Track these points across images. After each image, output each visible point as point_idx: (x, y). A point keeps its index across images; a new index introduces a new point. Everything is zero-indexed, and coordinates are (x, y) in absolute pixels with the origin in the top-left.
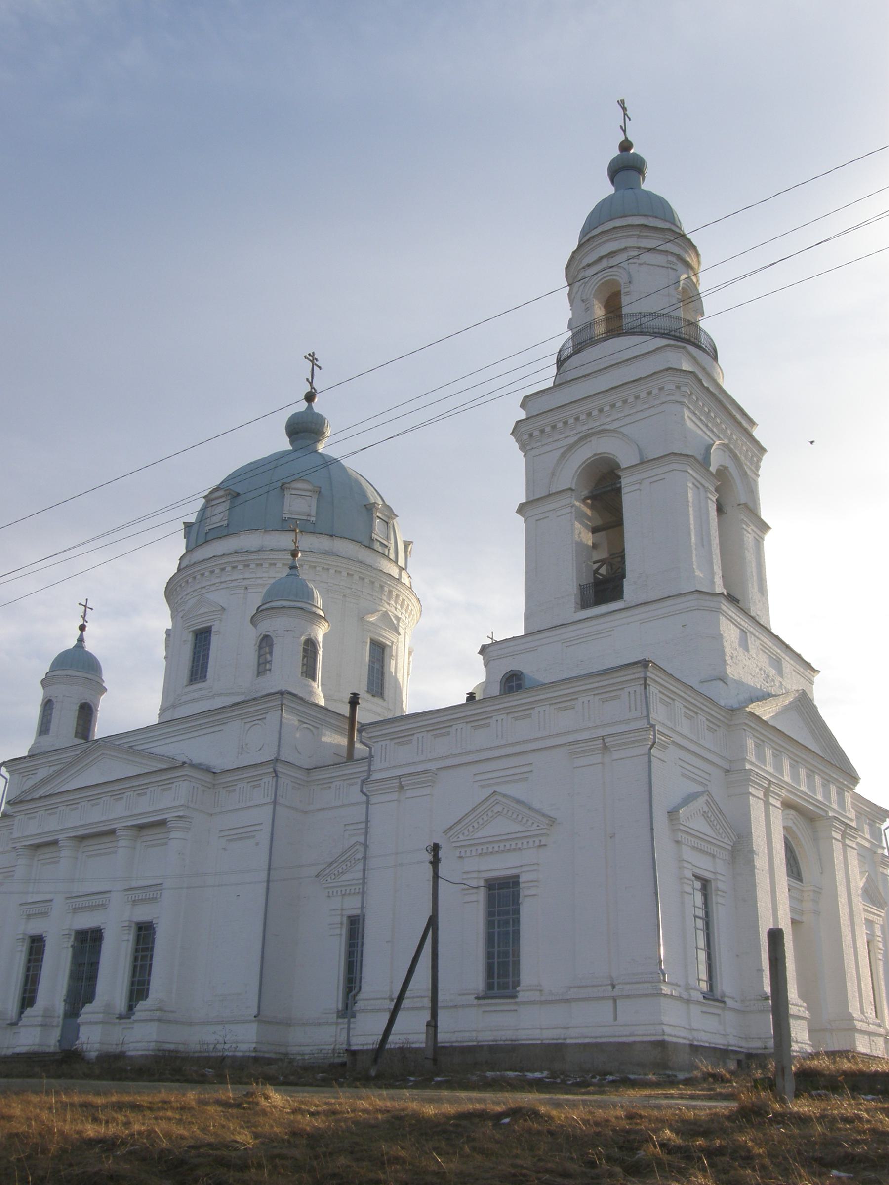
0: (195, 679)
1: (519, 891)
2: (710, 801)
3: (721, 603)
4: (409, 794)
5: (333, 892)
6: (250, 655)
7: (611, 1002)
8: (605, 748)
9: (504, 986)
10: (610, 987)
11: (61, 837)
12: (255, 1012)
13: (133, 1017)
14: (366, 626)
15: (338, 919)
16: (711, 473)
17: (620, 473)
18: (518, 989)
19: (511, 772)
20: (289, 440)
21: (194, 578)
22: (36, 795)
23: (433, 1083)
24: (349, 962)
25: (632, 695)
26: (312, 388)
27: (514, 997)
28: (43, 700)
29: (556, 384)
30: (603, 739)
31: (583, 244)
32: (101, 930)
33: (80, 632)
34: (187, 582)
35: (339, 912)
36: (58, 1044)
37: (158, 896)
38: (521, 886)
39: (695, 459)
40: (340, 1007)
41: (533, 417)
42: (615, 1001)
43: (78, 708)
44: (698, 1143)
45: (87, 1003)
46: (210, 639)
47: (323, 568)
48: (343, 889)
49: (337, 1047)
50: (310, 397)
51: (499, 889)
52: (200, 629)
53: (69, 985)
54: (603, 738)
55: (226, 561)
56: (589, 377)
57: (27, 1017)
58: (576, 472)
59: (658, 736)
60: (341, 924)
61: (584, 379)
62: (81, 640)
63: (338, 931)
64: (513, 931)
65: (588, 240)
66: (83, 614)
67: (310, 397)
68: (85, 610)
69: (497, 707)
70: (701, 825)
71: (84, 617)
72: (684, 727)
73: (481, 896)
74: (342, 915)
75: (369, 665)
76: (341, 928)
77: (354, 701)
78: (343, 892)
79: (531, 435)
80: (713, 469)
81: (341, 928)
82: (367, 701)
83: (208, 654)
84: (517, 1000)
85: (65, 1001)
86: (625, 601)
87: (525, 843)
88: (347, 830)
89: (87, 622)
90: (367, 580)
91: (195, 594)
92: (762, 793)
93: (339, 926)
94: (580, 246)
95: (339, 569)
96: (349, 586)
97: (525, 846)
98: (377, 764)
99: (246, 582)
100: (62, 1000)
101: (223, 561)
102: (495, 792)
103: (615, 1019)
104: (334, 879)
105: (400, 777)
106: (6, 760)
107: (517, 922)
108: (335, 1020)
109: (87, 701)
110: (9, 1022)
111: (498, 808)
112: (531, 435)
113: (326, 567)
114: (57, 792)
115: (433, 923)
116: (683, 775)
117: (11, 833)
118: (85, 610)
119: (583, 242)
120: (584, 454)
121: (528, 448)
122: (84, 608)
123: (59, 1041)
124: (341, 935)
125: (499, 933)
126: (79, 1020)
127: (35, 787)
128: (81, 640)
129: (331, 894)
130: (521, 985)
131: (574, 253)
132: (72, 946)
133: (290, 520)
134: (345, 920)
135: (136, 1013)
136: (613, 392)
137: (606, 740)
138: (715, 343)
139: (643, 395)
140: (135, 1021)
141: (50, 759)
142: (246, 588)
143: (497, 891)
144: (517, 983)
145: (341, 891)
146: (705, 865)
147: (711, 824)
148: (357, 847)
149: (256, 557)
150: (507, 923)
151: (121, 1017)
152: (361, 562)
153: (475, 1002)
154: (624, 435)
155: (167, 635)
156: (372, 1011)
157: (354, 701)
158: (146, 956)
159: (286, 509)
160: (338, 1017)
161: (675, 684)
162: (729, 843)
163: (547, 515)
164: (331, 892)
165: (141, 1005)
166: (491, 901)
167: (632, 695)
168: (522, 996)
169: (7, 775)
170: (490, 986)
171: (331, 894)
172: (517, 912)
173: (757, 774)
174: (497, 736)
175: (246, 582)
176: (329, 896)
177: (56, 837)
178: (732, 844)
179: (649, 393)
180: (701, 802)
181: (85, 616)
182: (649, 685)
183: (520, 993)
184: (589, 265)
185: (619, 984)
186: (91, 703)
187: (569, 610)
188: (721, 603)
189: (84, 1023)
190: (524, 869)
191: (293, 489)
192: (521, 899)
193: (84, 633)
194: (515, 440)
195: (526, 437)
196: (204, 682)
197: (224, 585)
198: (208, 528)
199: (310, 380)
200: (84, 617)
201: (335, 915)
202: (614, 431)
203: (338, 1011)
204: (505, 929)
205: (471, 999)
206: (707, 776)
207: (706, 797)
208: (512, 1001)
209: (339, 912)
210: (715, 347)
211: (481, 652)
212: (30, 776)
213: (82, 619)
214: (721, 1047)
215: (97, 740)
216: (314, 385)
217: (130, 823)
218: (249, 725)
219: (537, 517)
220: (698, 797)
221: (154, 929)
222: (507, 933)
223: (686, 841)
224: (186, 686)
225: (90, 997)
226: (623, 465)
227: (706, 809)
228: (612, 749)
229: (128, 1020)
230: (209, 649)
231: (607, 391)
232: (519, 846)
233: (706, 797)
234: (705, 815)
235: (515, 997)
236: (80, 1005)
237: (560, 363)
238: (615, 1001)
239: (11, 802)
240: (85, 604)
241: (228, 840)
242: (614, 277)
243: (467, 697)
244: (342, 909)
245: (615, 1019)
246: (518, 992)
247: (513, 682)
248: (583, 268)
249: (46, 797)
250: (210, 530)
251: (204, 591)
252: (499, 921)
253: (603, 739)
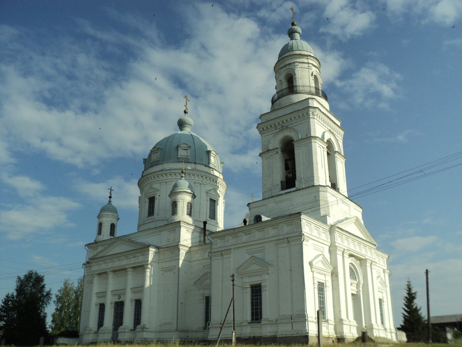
0: (150, 215)
1: (261, 289)
2: (323, 257)
3: (327, 189)
4: (225, 256)
5: (200, 288)
6: (169, 207)
7: (291, 324)
8: (288, 241)
9: (257, 319)
10: (290, 319)
11: (108, 271)
12: (176, 328)
13: (136, 330)
14: (208, 195)
15: (202, 298)
16: (325, 142)
17: (294, 143)
18: (262, 320)
19: (257, 249)
20: (179, 127)
21: (148, 179)
22: (99, 256)
23: (22, 288)
24: (206, 311)
25: (297, 224)
26: (186, 108)
27: (260, 322)
28: (98, 223)
29: (271, 110)
30: (287, 239)
31: (279, 60)
32: (123, 302)
33: (109, 199)
34: (146, 181)
35: (202, 295)
36: (111, 339)
37: (142, 290)
38: (262, 287)
39: (319, 138)
40: (204, 326)
41: (263, 123)
42: (292, 323)
43: (110, 225)
44: (75, 326)
45: (120, 326)
46: (154, 201)
47: (193, 175)
48: (204, 287)
49: (204, 339)
51: (255, 288)
52: (151, 197)
53: (114, 320)
54: (287, 238)
55: (159, 173)
56: (282, 109)
57: (101, 330)
58: (280, 140)
59: (305, 237)
60: (203, 299)
61: (281, 109)
62: (110, 201)
63: (202, 301)
64: (260, 308)
65: (281, 59)
66: (110, 192)
68: (111, 191)
69: (253, 227)
70: (320, 265)
71: (110, 193)
72: (315, 233)
73: (249, 290)
74: (203, 296)
75: (210, 208)
76: (203, 300)
77: (205, 223)
78: (204, 288)
79: (263, 129)
80: (325, 141)
81: (203, 300)
82: (209, 221)
83: (154, 206)
84: (261, 324)
85: (113, 325)
86: (296, 188)
87: (263, 273)
88: (204, 267)
89: (111, 195)
90: (208, 178)
91: (149, 185)
92: (341, 253)
93: (203, 300)
94: (278, 61)
95: (198, 175)
96: (202, 181)
97: (263, 274)
98: (214, 247)
99: (166, 181)
100: (111, 325)
101: (158, 174)
102: (253, 256)
103: (292, 329)
104: (200, 284)
105: (221, 251)
106: (87, 244)
107: (261, 299)
108: (202, 330)
109: (113, 223)
110: (95, 332)
111: (254, 261)
112: (263, 129)
113: (193, 174)
114: (106, 255)
115: (233, 299)
116: (314, 249)
117: (91, 269)
118: (111, 191)
119: (279, 59)
120: (281, 136)
121: (262, 133)
122: (112, 189)
123: (112, 338)
124: (203, 303)
125: (255, 302)
126: (118, 331)
127: (98, 254)
128: (110, 201)
129: (199, 289)
130: (263, 319)
131: (276, 63)
132: (114, 307)
133: (181, 158)
134: (204, 297)
135: (137, 329)
136: (290, 114)
137: (288, 239)
138: (326, 94)
139: (301, 115)
140: (136, 332)
141: (102, 244)
142: (166, 183)
143: (254, 289)
144: (261, 318)
145: (203, 288)
146: (321, 278)
147: (324, 265)
148: (208, 273)
149: (169, 172)
150: (257, 299)
151: (131, 330)
152: (206, 172)
153: (248, 324)
154: (295, 129)
155: (139, 199)
156: (215, 328)
157: (205, 223)
158: (139, 310)
159: (179, 154)
160: (203, 330)
161: (311, 219)
162: (330, 270)
163: (269, 157)
164: (199, 288)
165: (138, 327)
166: (252, 292)
167: (297, 224)
168: (263, 322)
169: (88, 249)
170: (252, 319)
171: (199, 289)
172: (261, 295)
173: (340, 247)
174: (253, 237)
175: (166, 181)
176: (199, 290)
177: (106, 271)
178: (331, 271)
179: (303, 115)
180: (320, 258)
182: (302, 220)
183: (262, 321)
184: (282, 68)
185: (294, 318)
186: (114, 223)
187: (278, 190)
188: (327, 189)
189: (119, 332)
190: (263, 281)
191: (181, 147)
192: (262, 291)
193: (111, 199)
194: (257, 130)
195: (261, 129)
196: (153, 216)
197: (158, 182)
198: (152, 161)
199: (186, 105)
200: (110, 193)
201: (148, 237)
202: (291, 128)
203: (203, 328)
204: (257, 301)
205: (246, 324)
206: (323, 249)
207: (322, 256)
208: (260, 324)
209: (202, 295)
210: (326, 96)
211: (248, 205)
212: (96, 249)
213: (110, 194)
214: (327, 336)
215: (118, 237)
216: (187, 107)
217: (131, 266)
218: (170, 232)
219: (266, 158)
220: (319, 256)
221: (141, 301)
222: (257, 302)
223: (315, 271)
224: (147, 217)
225: (121, 324)
226: (295, 140)
227: (322, 260)
228: (290, 242)
229: (134, 331)
230: (154, 204)
231: (289, 114)
232: (261, 274)
233: (322, 256)
234: (322, 262)
235: (261, 323)
236: (118, 326)
237: (273, 102)
238: (292, 323)
239: (90, 259)
240: (110, 189)
241: (164, 272)
242: (291, 72)
243: (244, 221)
244: (203, 294)
245: (292, 329)
246: (261, 321)
247: (258, 293)
248: (280, 69)
249: (102, 257)
250: (153, 162)
251: (152, 184)
252: (255, 298)
253: (287, 239)
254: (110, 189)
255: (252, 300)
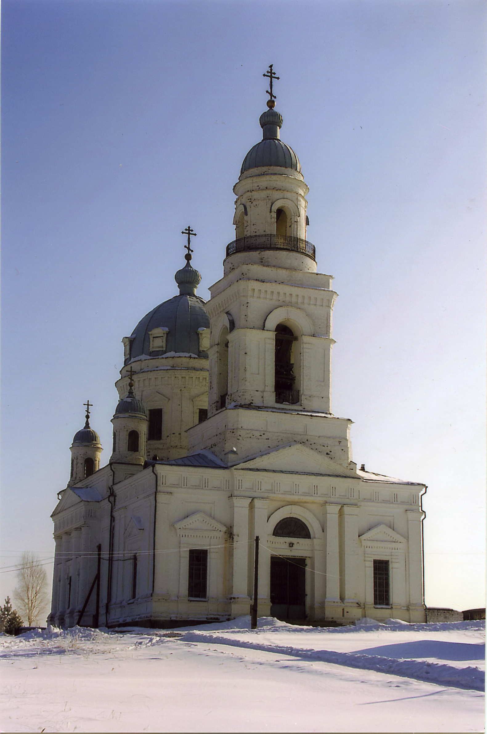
50: (188, 257)
62: (87, 423)
67: (188, 257)
122: (89, 404)
128: (87, 423)
181: (88, 410)
200: (87, 411)
254: (87, 404)
255: (375, 591)
